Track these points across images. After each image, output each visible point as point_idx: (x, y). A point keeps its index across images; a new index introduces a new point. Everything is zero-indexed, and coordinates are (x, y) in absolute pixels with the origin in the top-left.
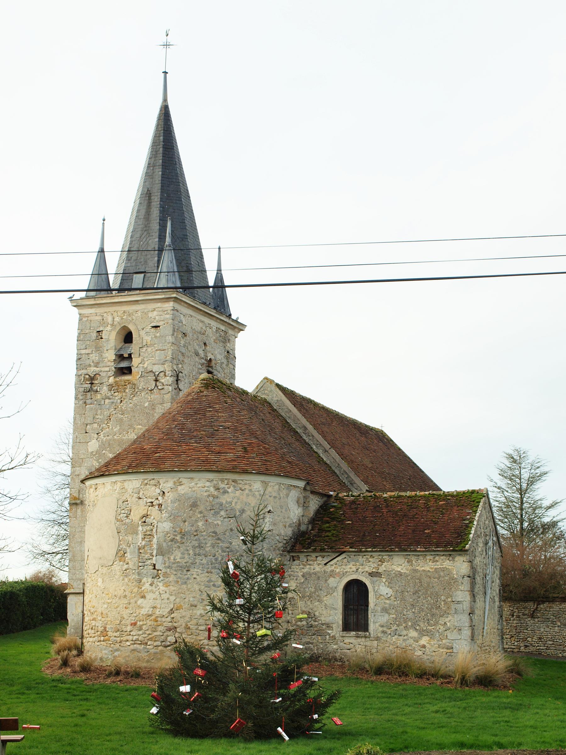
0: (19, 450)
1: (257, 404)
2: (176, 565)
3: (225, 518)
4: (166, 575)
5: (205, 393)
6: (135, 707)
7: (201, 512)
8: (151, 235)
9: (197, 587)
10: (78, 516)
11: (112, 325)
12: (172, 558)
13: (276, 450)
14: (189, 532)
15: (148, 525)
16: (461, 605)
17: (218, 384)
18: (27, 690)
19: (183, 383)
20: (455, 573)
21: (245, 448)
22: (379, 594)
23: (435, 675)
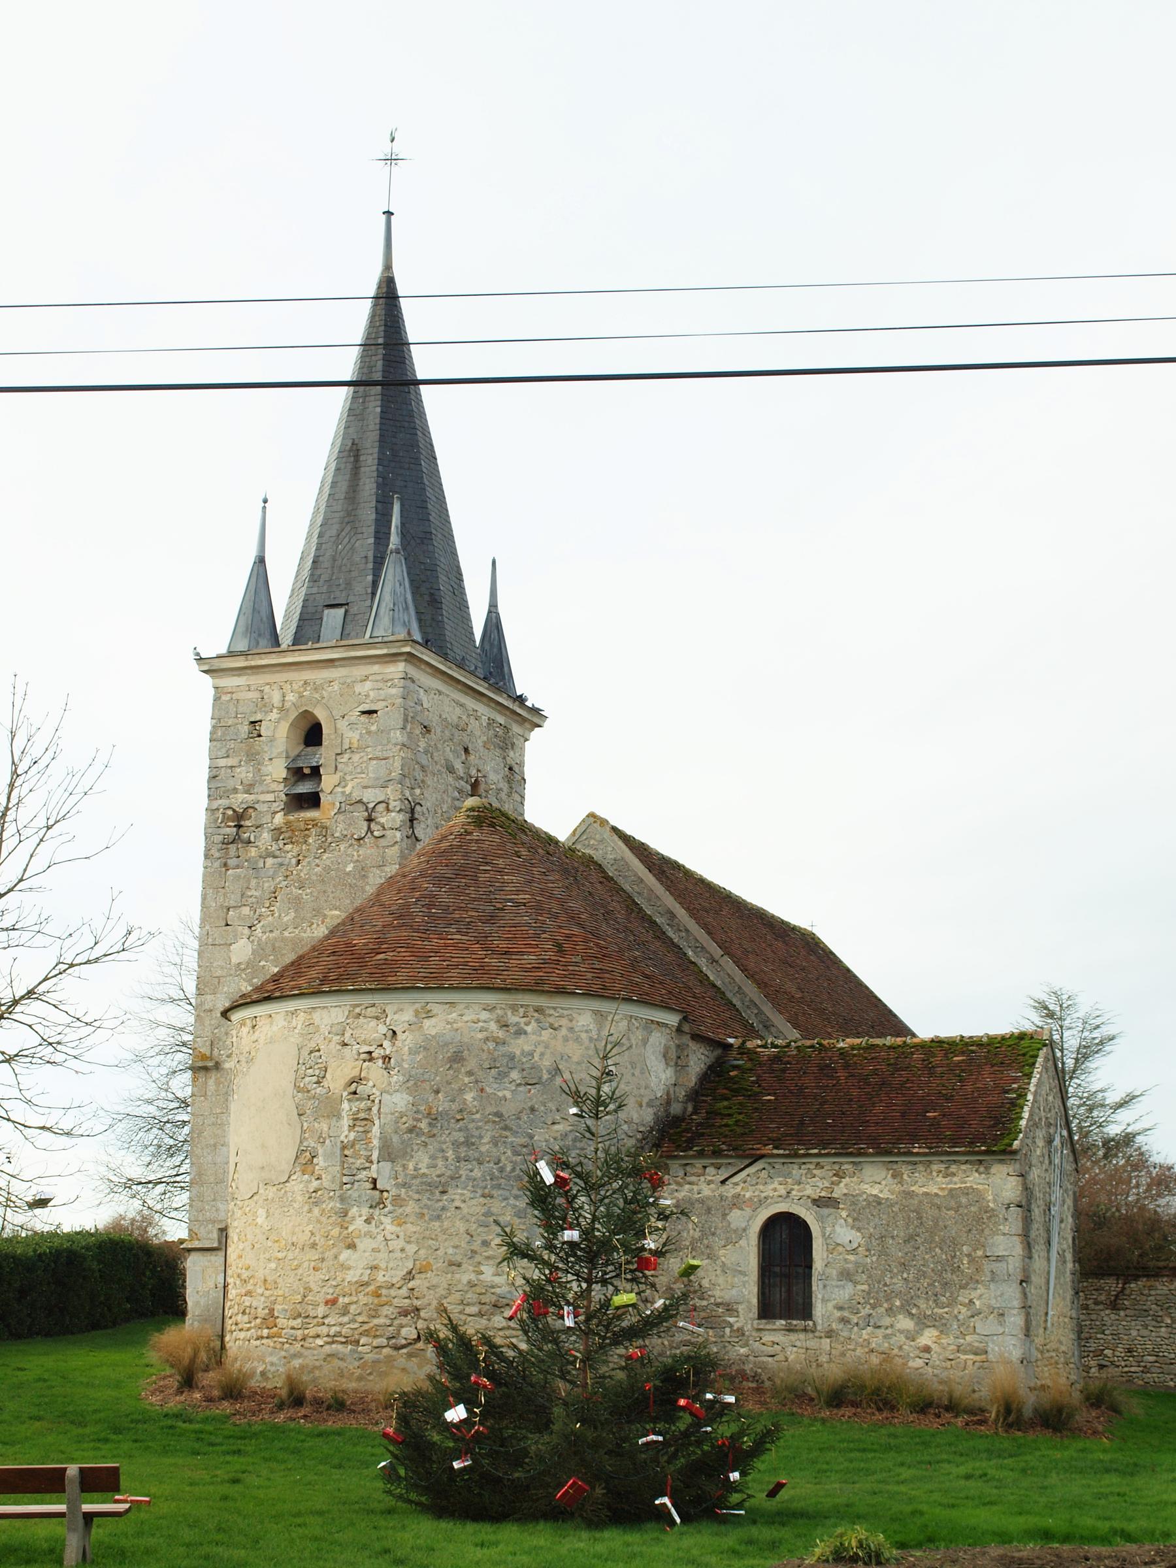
0: (111, 923)
1: (576, 865)
2: (419, 1180)
3: (520, 1085)
4: (398, 1201)
5: (476, 835)
6: (340, 1466)
7: (470, 1073)
8: (359, 530)
9: (461, 1226)
10: (209, 1093)
12: (411, 1166)
13: (621, 951)
14: (446, 1113)
16: (1004, 1265)
17: (501, 825)
18: (115, 1433)
19: (423, 826)
20: (990, 1198)
21: (559, 946)
22: (834, 1241)
23: (952, 1407)
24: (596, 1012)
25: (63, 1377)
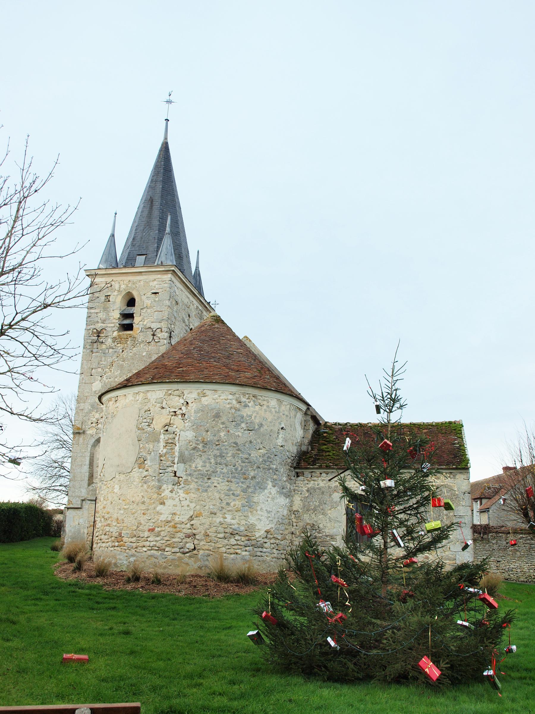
2: (197, 473)
4: (186, 482)
5: (216, 326)
7: (223, 423)
9: (217, 495)
11: (119, 291)
12: (194, 466)
15: (171, 434)
18: (44, 595)
24: (278, 400)
25: (14, 562)
